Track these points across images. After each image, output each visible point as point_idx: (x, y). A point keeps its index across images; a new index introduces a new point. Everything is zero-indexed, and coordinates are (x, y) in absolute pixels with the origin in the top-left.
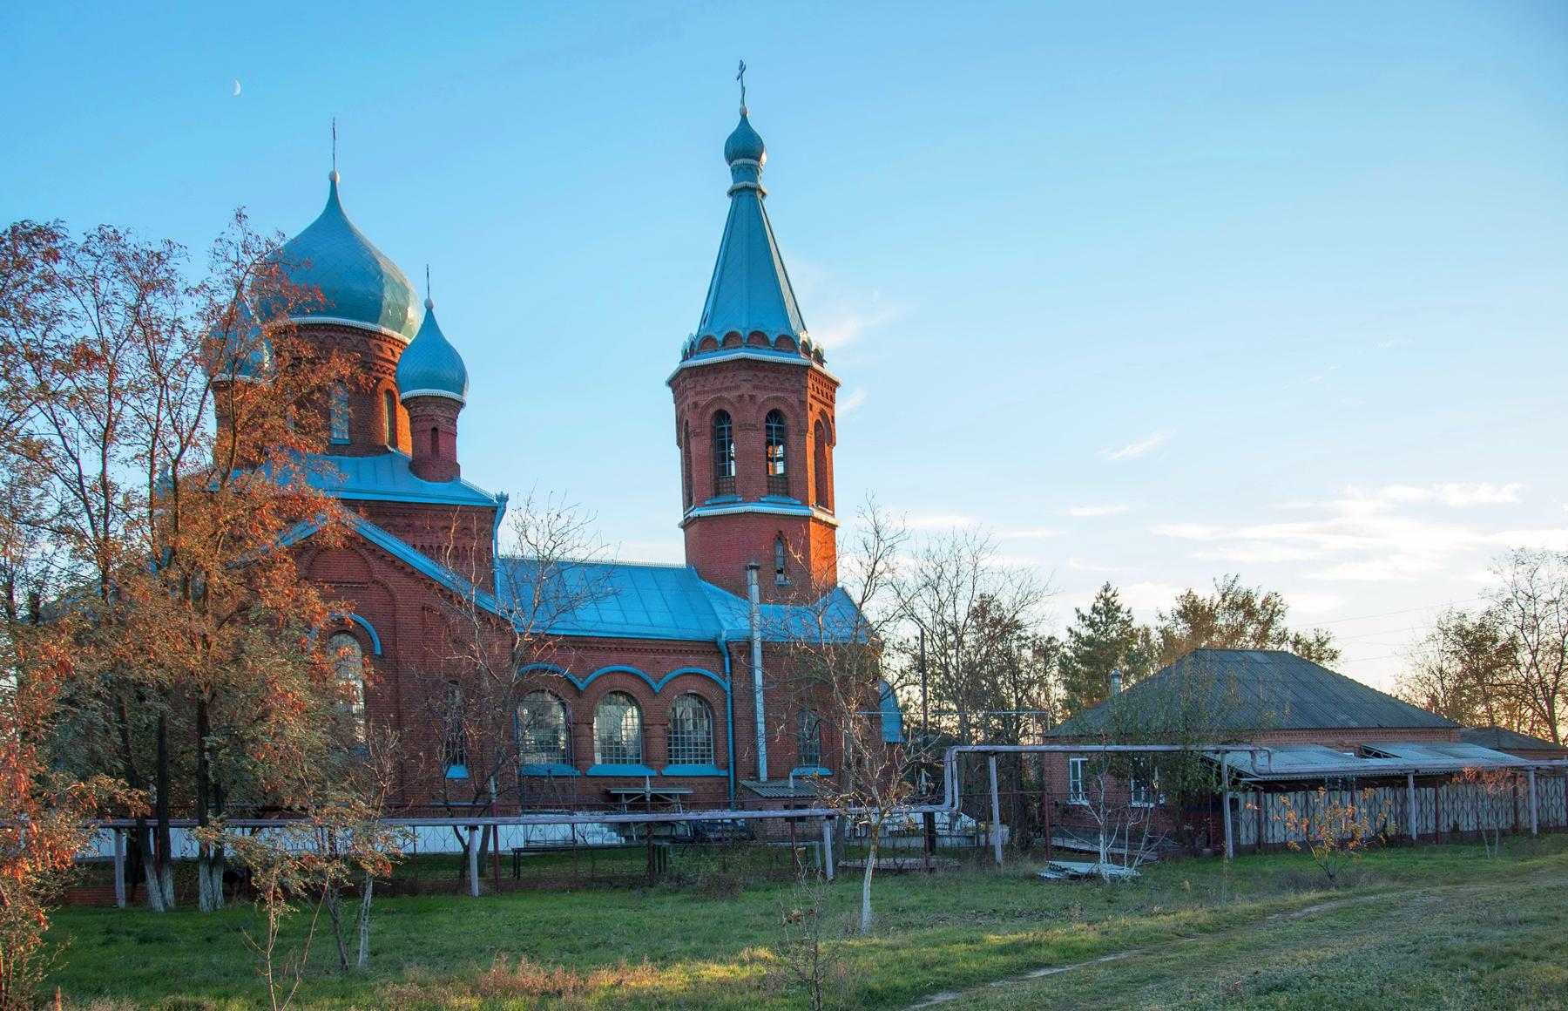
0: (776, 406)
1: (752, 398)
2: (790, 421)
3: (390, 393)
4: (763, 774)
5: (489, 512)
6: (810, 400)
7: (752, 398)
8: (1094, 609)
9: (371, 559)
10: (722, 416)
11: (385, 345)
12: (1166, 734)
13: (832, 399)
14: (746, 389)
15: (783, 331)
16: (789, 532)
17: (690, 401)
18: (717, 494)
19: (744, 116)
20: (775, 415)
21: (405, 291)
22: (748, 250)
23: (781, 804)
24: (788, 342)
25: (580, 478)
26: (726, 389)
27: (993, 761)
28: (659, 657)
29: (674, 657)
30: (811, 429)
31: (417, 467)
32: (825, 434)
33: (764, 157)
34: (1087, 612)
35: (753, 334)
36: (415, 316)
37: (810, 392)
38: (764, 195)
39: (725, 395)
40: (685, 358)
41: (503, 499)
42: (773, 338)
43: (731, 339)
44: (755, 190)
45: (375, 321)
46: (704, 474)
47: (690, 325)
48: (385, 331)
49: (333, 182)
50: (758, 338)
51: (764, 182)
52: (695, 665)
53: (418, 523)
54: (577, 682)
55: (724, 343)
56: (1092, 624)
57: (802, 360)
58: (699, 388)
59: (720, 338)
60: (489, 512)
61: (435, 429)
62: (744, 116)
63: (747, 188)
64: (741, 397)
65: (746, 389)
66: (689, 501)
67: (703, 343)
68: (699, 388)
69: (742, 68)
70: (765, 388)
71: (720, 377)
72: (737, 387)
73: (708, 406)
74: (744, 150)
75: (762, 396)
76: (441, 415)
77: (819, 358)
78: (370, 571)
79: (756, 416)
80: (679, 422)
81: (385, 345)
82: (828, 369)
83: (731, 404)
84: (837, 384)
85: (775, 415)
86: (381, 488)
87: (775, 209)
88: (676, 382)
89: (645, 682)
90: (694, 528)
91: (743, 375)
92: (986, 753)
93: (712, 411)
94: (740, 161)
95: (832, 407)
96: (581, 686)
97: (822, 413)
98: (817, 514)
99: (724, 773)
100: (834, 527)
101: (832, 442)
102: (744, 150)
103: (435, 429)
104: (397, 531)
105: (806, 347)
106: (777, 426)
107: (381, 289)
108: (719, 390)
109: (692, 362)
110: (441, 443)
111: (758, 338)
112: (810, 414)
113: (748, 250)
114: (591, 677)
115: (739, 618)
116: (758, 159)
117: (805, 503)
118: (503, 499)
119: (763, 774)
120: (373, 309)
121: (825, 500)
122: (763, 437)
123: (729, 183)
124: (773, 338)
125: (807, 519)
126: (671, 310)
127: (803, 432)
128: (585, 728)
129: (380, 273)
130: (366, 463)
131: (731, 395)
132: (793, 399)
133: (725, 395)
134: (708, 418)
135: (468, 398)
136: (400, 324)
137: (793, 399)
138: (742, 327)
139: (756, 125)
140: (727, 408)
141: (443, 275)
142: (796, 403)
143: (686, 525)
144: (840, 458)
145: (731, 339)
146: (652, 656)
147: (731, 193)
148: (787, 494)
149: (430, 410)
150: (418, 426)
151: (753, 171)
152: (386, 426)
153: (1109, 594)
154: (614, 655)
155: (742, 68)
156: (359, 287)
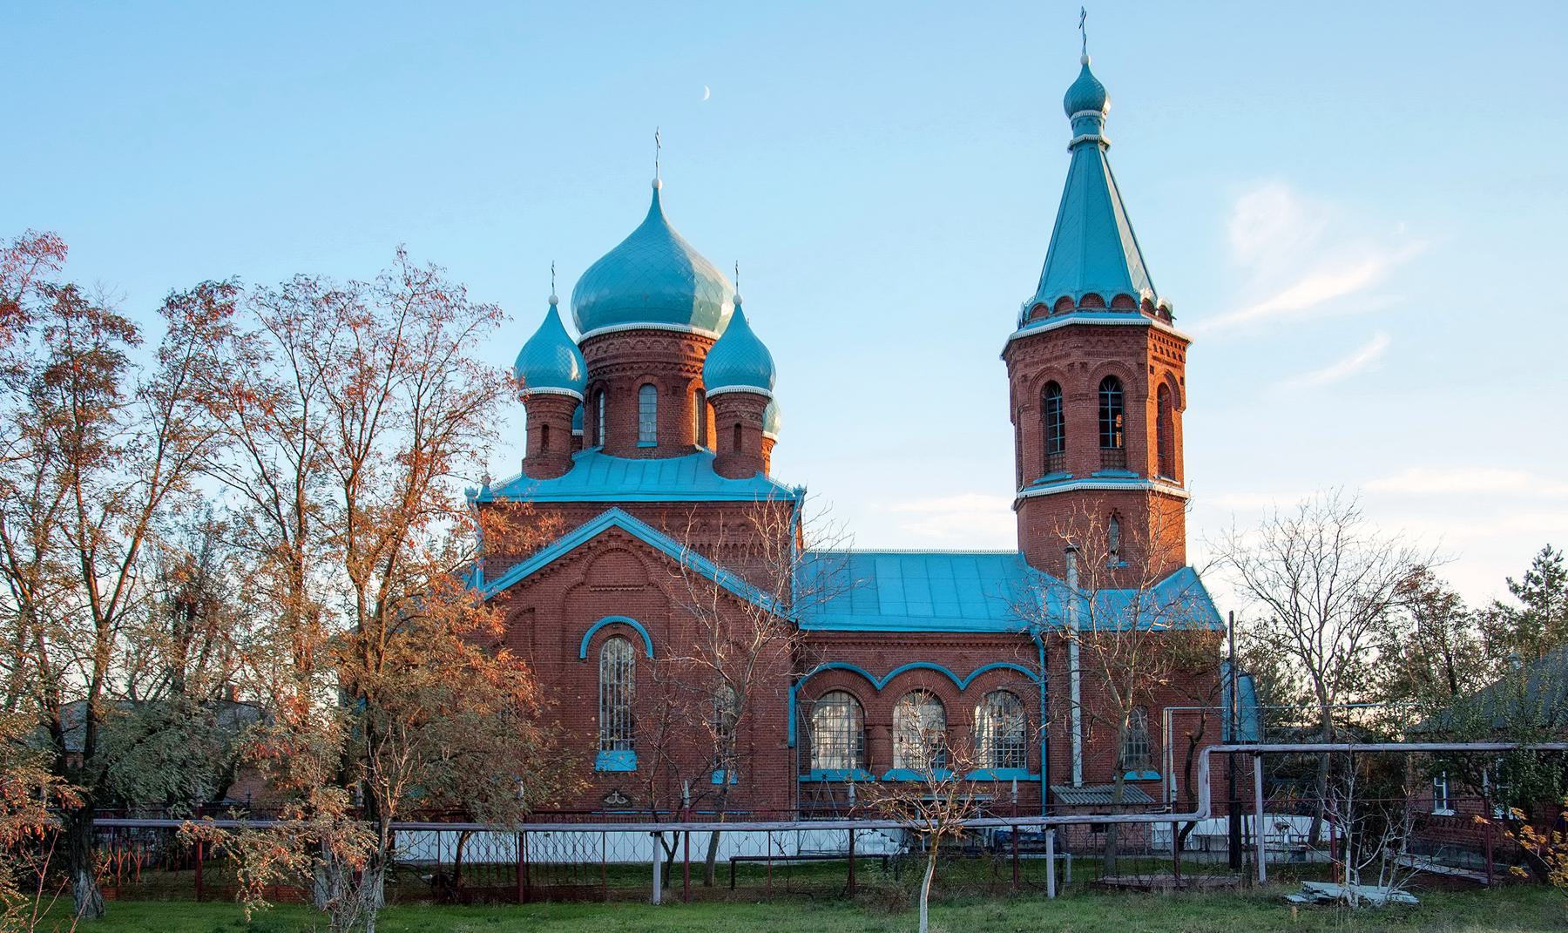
0: (1112, 372)
1: (1084, 365)
2: (1128, 387)
3: (701, 392)
4: (1078, 780)
5: (791, 504)
6: (1150, 362)
7: (1084, 365)
8: (1529, 577)
9: (647, 561)
10: (1052, 387)
11: (697, 345)
12: (1501, 732)
13: (1181, 359)
14: (1077, 357)
15: (1121, 290)
16: (1125, 512)
17: (1019, 374)
18: (1103, 467)
19: (1085, 66)
20: (1110, 381)
21: (718, 287)
22: (1089, 205)
23: (1091, 810)
24: (1126, 301)
25: (901, 467)
26: (1056, 358)
27: (1257, 762)
28: (966, 652)
29: (983, 651)
30: (1153, 392)
31: (720, 466)
32: (1171, 397)
33: (1107, 106)
34: (1520, 581)
35: (1086, 297)
36: (727, 310)
37: (1150, 354)
38: (1107, 146)
39: (1055, 364)
40: (1023, 323)
41: (801, 492)
42: (1108, 299)
43: (1063, 304)
44: (1096, 142)
45: (686, 321)
46: (1036, 454)
47: (1028, 292)
48: (695, 330)
49: (656, 190)
50: (1092, 300)
51: (1105, 135)
52: (1015, 658)
53: (714, 522)
54: (874, 680)
55: (1056, 309)
56: (1528, 597)
57: (1144, 318)
58: (1028, 360)
59: (1051, 304)
60: (791, 504)
61: (738, 426)
62: (1085, 66)
63: (1086, 141)
64: (1072, 365)
65: (1077, 357)
66: (1023, 479)
67: (1035, 311)
68: (1028, 360)
69: (1084, 15)
70: (1098, 354)
71: (1050, 345)
72: (1068, 355)
73: (1037, 378)
74: (1085, 101)
75: (1094, 363)
76: (744, 411)
77: (1166, 315)
78: (646, 572)
79: (1088, 384)
80: (1013, 397)
81: (697, 345)
82: (1178, 328)
83: (1062, 373)
84: (1187, 342)
85: (1110, 381)
86: (678, 488)
87: (1120, 163)
88: (1014, 351)
89: (948, 678)
90: (1023, 510)
91: (1074, 341)
92: (1251, 752)
93: (1042, 382)
94: (1080, 114)
95: (1181, 368)
96: (879, 686)
97: (1169, 375)
98: (1160, 487)
99: (1035, 777)
100: (1181, 499)
101: (1180, 405)
102: (1085, 101)
103: (738, 426)
104: (674, 531)
105: (1149, 306)
106: (1113, 396)
107: (693, 289)
108: (1049, 360)
109: (1025, 332)
110: (745, 442)
111: (1092, 300)
112: (1150, 377)
113: (1089, 205)
114: (891, 675)
115: (1067, 607)
116: (1100, 108)
117: (1144, 475)
118: (801, 492)
119: (1078, 780)
120: (684, 310)
121: (1169, 466)
122: (1095, 406)
123: (1069, 136)
124: (1108, 299)
125: (1143, 492)
126: (1006, 275)
127: (1142, 398)
128: (883, 731)
129: (691, 274)
130: (671, 464)
131: (1061, 365)
132: (1131, 363)
133: (1055, 364)
134: (1038, 390)
135: (775, 393)
136: (712, 323)
137: (1131, 363)
138: (1074, 292)
139: (1097, 72)
140: (1057, 378)
141: (747, 276)
142: (1134, 367)
143: (1018, 506)
144: (1193, 425)
145: (1063, 304)
146: (958, 651)
147: (1071, 148)
148: (1125, 467)
149: (732, 407)
150: (723, 424)
151: (1094, 123)
152: (695, 425)
153: (1551, 558)
154: (917, 651)
155: (1084, 15)
156: (669, 290)
